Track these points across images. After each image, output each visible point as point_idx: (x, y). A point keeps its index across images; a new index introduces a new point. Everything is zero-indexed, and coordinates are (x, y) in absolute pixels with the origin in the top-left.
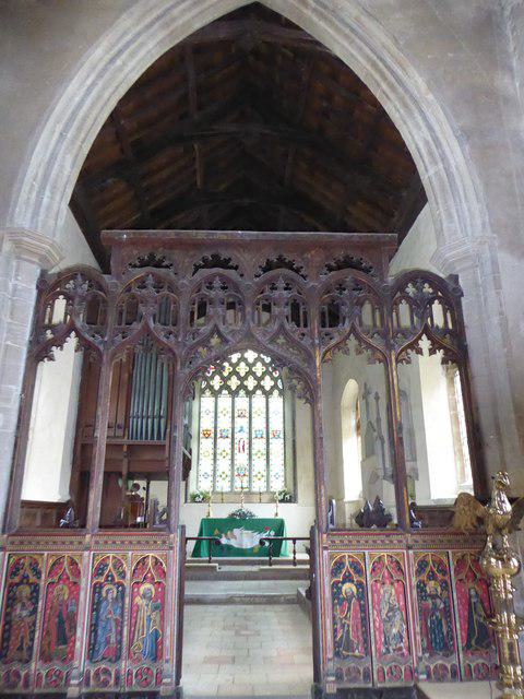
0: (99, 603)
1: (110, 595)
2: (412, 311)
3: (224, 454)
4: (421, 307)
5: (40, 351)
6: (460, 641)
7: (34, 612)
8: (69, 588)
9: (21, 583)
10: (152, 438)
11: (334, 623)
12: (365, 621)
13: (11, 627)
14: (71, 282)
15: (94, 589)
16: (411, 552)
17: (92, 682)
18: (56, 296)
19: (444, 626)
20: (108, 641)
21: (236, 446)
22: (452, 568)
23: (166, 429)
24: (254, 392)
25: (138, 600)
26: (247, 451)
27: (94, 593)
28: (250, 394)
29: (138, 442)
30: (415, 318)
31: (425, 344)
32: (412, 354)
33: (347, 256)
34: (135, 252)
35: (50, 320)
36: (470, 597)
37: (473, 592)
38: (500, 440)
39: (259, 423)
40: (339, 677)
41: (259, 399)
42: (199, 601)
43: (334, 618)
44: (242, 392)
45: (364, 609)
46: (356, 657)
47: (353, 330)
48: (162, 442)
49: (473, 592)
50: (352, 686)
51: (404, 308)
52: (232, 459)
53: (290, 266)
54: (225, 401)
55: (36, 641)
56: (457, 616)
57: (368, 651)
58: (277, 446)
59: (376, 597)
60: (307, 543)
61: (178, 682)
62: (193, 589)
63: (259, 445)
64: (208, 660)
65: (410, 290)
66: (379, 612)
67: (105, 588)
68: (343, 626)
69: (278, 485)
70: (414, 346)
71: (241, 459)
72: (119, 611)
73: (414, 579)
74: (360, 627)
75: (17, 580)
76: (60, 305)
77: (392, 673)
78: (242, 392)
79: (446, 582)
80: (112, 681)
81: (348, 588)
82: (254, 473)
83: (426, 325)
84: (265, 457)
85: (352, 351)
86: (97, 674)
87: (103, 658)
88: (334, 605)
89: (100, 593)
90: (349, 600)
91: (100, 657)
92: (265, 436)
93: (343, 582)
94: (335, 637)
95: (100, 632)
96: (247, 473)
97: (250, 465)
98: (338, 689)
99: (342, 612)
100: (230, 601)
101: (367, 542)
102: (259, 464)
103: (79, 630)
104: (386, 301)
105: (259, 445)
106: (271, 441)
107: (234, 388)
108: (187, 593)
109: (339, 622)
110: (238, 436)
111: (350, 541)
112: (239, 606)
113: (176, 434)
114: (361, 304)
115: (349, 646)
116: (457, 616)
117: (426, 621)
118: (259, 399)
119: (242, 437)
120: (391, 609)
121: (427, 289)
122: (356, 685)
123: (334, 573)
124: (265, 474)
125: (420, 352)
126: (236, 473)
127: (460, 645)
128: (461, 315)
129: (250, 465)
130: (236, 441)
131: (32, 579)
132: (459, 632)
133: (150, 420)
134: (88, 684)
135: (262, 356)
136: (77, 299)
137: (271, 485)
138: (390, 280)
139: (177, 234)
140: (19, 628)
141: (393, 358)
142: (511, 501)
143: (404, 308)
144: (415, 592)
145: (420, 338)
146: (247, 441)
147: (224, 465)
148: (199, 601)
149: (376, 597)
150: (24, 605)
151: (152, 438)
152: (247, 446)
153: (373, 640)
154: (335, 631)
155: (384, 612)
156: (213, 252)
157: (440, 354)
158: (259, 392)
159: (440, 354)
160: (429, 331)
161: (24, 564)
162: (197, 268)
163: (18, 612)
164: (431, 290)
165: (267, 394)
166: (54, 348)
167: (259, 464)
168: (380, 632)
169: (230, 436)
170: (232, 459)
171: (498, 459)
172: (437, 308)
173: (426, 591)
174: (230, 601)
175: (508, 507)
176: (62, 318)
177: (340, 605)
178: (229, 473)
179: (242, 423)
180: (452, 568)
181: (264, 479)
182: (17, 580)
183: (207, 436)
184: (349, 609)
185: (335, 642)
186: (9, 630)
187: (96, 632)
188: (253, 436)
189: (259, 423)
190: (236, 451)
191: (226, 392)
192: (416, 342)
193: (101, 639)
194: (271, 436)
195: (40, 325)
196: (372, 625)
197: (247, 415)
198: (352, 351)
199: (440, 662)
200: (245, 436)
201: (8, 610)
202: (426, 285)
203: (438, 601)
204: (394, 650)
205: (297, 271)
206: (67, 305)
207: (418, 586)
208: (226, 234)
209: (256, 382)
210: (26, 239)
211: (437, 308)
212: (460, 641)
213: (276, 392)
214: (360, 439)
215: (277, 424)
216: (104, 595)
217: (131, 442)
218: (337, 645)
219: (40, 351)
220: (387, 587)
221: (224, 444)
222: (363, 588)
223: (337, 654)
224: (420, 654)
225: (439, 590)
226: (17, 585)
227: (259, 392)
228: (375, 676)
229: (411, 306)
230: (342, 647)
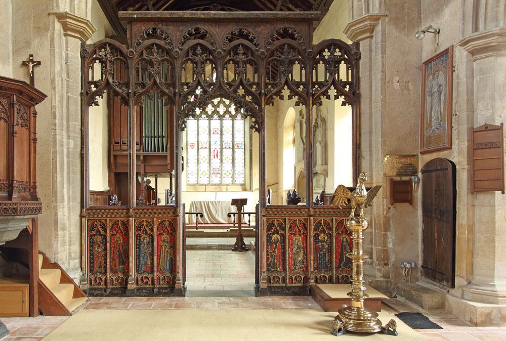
0: (140, 245)
1: (145, 241)
2: (326, 69)
3: (204, 159)
4: (332, 66)
5: (88, 99)
6: (334, 264)
7: (105, 249)
8: (123, 237)
9: (96, 234)
10: (159, 151)
11: (267, 255)
12: (284, 254)
13: (93, 256)
14: (103, 50)
15: (137, 237)
16: (312, 218)
17: (139, 283)
18: (94, 61)
19: (327, 257)
20: (146, 264)
21: (212, 154)
22: (334, 227)
23: (167, 144)
24: (223, 116)
25: (161, 243)
26: (219, 157)
27: (137, 239)
28: (221, 117)
29: (150, 153)
30: (328, 74)
31: (332, 92)
32: (324, 99)
33: (285, 29)
34: (143, 28)
35: (93, 78)
36: (343, 242)
37: (345, 240)
38: (371, 155)
39: (227, 138)
40: (269, 281)
41: (227, 122)
42: (193, 248)
43: (267, 252)
44: (216, 116)
45: (284, 248)
46: (278, 271)
47: (287, 83)
48: (165, 153)
49: (345, 240)
50: (275, 285)
51: (321, 67)
52: (210, 163)
53: (246, 37)
54: (204, 122)
55: (108, 263)
56: (334, 252)
57: (285, 269)
58: (239, 153)
59: (291, 242)
60: (255, 215)
61: (184, 284)
62: (190, 241)
63: (227, 153)
64: (198, 276)
65: (326, 54)
66: (292, 249)
67: (143, 237)
68: (272, 256)
69: (240, 180)
70: (325, 94)
71: (216, 162)
72: (150, 249)
73: (312, 233)
74: (281, 256)
75: (94, 233)
76: (97, 66)
77: (297, 280)
78: (216, 116)
79: (330, 235)
80: (150, 283)
81: (276, 237)
82: (224, 172)
83: (334, 79)
84: (231, 161)
85: (286, 97)
86: (142, 279)
87: (144, 272)
88: (267, 245)
89: (140, 240)
90: (276, 243)
91: (142, 271)
92: (231, 147)
93: (273, 234)
94: (267, 261)
95: (141, 259)
96: (220, 172)
97: (221, 166)
98: (268, 287)
99: (272, 249)
100: (209, 248)
101: (287, 212)
102: (228, 166)
103: (131, 258)
104: (310, 63)
105: (227, 153)
106: (235, 150)
107: (210, 113)
108: (187, 243)
109: (269, 254)
110: (213, 148)
111: (278, 212)
112: (215, 251)
113: (59, 70)
114: (292, 63)
115: (275, 266)
116: (334, 252)
117: (317, 253)
118: (227, 122)
119: (216, 146)
120: (298, 248)
121: (338, 53)
122: (278, 285)
123: (268, 229)
124: (231, 172)
125: (328, 97)
126: (212, 172)
127: (334, 266)
128: (358, 72)
129: (221, 166)
130: (212, 150)
131: (102, 232)
132: (334, 260)
133: (149, 139)
134: (137, 284)
135: (224, 99)
136: (108, 64)
137: (235, 179)
138: (315, 42)
139: (170, 14)
140: (98, 257)
141: (311, 102)
142: (367, 189)
143: (321, 67)
144: (312, 239)
145: (329, 88)
146: (219, 150)
147: (204, 166)
148: (193, 248)
149: (291, 242)
150: (99, 246)
151: (159, 151)
152: (219, 154)
153: (287, 263)
154: (267, 259)
155: (295, 249)
156: (195, 26)
157: (342, 99)
158: (227, 116)
159: (296, 99)
160: (336, 83)
161: (96, 225)
162: (186, 39)
163: (96, 249)
164: (340, 54)
165: (233, 118)
166: (97, 97)
167: (228, 166)
168: (292, 260)
169: (208, 147)
170: (210, 163)
171: (368, 166)
172: (343, 67)
173: (318, 239)
174: (209, 248)
175: (365, 193)
176: (100, 78)
177: (271, 245)
178: (208, 172)
179: (216, 138)
180: (334, 227)
181: (231, 176)
182: (94, 233)
183: (192, 146)
184: (276, 248)
185: (267, 264)
186: (93, 258)
187: (139, 259)
188: (224, 147)
189: (227, 138)
190: (212, 157)
191: (205, 116)
192: (326, 91)
193: (142, 262)
194: (236, 147)
195: (86, 82)
196: (287, 256)
197: (219, 132)
198: (286, 97)
199: (323, 274)
200: (218, 147)
201: (91, 248)
202: (337, 50)
203: (325, 244)
204: (299, 268)
205: (251, 41)
206: (102, 67)
207: (314, 236)
208: (203, 14)
209: (225, 109)
210: (68, 20)
211: (343, 67)
212: (334, 264)
213: (239, 116)
214: (295, 148)
215: (239, 138)
216: (142, 240)
217: (145, 153)
218: (268, 265)
219: (88, 99)
220: (297, 236)
221: (204, 153)
222: (284, 237)
223: (268, 270)
224: (312, 270)
225: (326, 238)
226: (94, 235)
227: (227, 116)
228: (287, 281)
229: (326, 66)
230: (270, 266)
